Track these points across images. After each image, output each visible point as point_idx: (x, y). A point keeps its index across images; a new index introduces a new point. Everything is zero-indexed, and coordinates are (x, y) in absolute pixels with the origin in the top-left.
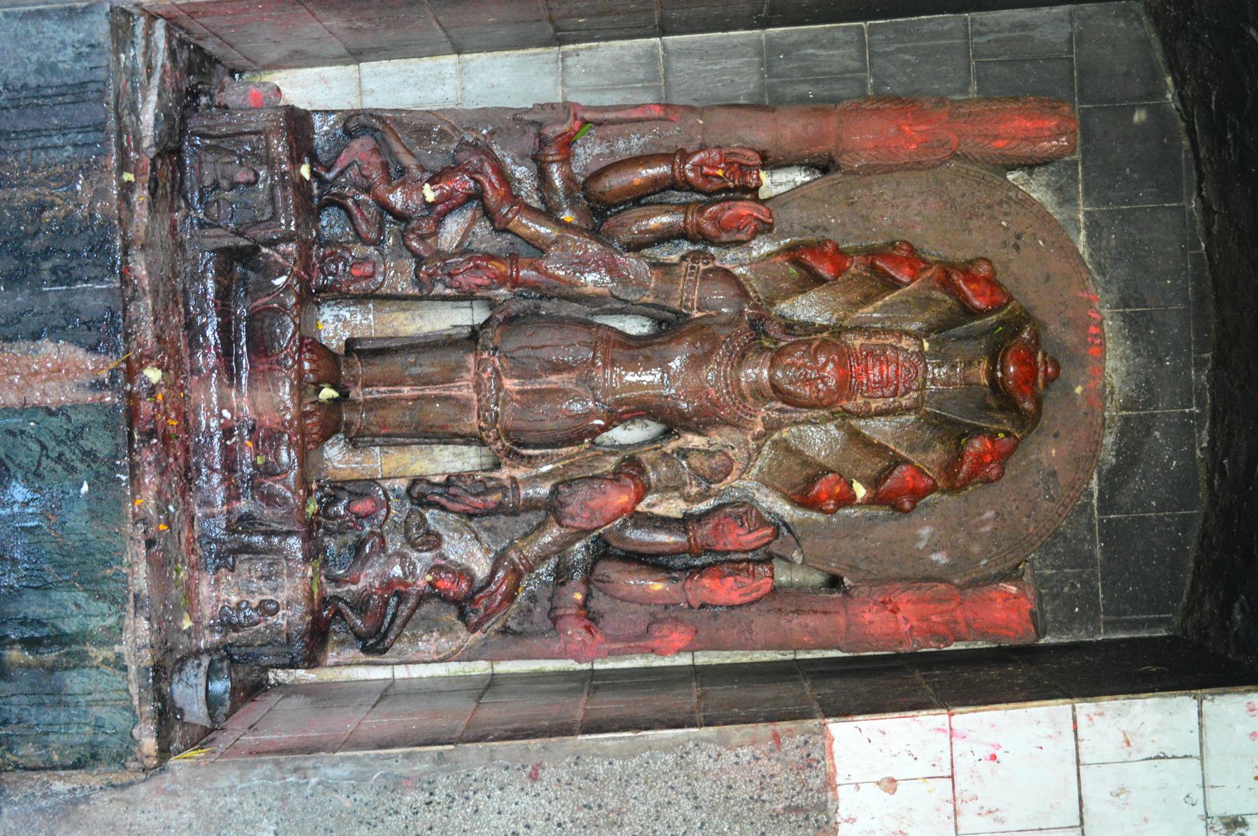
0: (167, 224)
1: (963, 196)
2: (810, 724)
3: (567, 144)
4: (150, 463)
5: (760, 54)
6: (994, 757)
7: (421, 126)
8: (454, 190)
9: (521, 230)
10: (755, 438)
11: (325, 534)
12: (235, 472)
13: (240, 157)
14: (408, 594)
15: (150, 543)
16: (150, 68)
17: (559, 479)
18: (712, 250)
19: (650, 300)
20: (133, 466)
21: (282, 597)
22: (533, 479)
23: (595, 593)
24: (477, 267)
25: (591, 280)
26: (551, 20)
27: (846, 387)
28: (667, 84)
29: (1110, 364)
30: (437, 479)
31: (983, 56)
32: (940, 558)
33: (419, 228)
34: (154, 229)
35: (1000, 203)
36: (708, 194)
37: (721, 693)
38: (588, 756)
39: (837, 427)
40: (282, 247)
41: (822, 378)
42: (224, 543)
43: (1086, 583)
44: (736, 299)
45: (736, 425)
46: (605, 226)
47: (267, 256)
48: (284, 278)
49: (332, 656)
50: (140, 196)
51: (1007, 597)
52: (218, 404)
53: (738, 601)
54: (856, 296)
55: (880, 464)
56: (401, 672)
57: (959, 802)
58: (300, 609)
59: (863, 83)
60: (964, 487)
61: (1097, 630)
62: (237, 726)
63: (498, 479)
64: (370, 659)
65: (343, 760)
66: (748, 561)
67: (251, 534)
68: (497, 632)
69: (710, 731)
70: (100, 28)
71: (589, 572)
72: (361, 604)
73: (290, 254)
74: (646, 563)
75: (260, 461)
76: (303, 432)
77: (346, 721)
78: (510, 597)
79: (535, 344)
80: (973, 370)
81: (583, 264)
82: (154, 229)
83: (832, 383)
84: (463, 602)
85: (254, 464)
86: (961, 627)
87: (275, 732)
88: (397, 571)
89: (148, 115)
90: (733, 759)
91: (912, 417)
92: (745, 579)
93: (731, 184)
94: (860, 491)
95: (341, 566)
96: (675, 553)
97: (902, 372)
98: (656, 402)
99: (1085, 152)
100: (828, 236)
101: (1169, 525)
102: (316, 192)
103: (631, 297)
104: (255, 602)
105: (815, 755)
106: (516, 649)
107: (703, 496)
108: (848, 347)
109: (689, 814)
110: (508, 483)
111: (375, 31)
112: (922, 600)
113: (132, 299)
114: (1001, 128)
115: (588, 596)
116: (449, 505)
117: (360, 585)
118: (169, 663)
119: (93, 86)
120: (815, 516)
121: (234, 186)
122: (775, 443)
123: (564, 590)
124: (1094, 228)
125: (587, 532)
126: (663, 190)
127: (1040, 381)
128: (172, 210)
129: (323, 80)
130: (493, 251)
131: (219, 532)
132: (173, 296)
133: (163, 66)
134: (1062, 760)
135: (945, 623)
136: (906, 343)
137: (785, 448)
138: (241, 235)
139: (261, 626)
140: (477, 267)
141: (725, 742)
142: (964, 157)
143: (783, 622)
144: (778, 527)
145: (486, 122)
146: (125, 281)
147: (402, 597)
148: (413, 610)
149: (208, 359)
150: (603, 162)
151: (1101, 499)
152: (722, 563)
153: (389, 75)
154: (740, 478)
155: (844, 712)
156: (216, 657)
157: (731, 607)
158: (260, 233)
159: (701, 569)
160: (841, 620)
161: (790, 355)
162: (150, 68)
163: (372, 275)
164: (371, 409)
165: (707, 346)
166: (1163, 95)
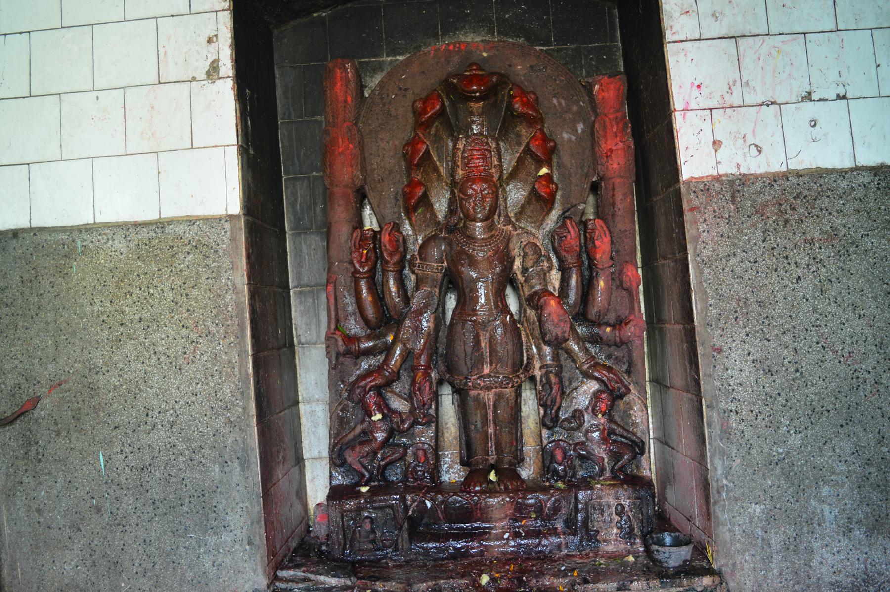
2: (683, 190)
3: (350, 339)
4: (538, 581)
5: (299, 234)
6: (699, 86)
7: (339, 425)
8: (375, 403)
9: (398, 364)
10: (516, 230)
11: (575, 478)
15: (586, 581)
16: (305, 580)
17: (541, 341)
18: (408, 257)
19: (437, 290)
21: (613, 502)
22: (540, 356)
23: (605, 321)
26: (279, 349)
27: (486, 179)
28: (316, 285)
29: (469, 39)
30: (542, 412)
32: (580, 127)
33: (397, 423)
34: (399, 579)
35: (382, 99)
36: (377, 259)
37: (662, 245)
38: (706, 319)
39: (508, 185)
40: (409, 503)
41: (481, 191)
42: (582, 536)
45: (508, 239)
46: (395, 317)
48: (427, 502)
49: (646, 473)
51: (601, 90)
52: (501, 541)
53: (609, 238)
54: (434, 176)
55: (529, 160)
57: (725, 106)
59: (316, 177)
62: (687, 528)
66: (585, 232)
67: (577, 521)
68: (629, 377)
69: (690, 247)
72: (615, 456)
73: (412, 498)
74: (588, 292)
75: (534, 516)
76: (516, 491)
78: (610, 369)
80: (475, 111)
81: (417, 329)
82: (399, 579)
83: (484, 186)
84: (613, 395)
85: (535, 519)
86: (619, 115)
87: (693, 506)
88: (596, 435)
89: (333, 581)
90: (705, 234)
92: (597, 234)
94: (544, 171)
95: (593, 468)
96: (582, 275)
97: (477, 147)
98: (496, 285)
100: (400, 192)
103: (436, 301)
104: (617, 518)
106: (639, 365)
107: (549, 259)
108: (463, 178)
110: (544, 371)
111: (285, 450)
112: (605, 137)
114: (341, 99)
115: (608, 324)
116: (557, 404)
117: (605, 456)
118: (656, 569)
120: (558, 197)
121: (373, 531)
122: (517, 220)
123: (605, 338)
124: (394, 52)
125: (571, 325)
126: (375, 285)
128: (387, 567)
129: (313, 480)
130: (410, 381)
131: (577, 540)
133: (304, 572)
138: (402, 527)
139: (631, 514)
140: (419, 389)
141: (696, 239)
143: (620, 213)
144: (566, 217)
145: (337, 385)
147: (612, 432)
148: (619, 426)
149: (474, 546)
151: (543, 46)
153: (310, 442)
156: (651, 541)
157: (612, 242)
158: (401, 516)
159: (591, 259)
160: (617, 181)
161: (468, 210)
162: (305, 580)
163: (424, 450)
164: (502, 451)
165: (464, 257)
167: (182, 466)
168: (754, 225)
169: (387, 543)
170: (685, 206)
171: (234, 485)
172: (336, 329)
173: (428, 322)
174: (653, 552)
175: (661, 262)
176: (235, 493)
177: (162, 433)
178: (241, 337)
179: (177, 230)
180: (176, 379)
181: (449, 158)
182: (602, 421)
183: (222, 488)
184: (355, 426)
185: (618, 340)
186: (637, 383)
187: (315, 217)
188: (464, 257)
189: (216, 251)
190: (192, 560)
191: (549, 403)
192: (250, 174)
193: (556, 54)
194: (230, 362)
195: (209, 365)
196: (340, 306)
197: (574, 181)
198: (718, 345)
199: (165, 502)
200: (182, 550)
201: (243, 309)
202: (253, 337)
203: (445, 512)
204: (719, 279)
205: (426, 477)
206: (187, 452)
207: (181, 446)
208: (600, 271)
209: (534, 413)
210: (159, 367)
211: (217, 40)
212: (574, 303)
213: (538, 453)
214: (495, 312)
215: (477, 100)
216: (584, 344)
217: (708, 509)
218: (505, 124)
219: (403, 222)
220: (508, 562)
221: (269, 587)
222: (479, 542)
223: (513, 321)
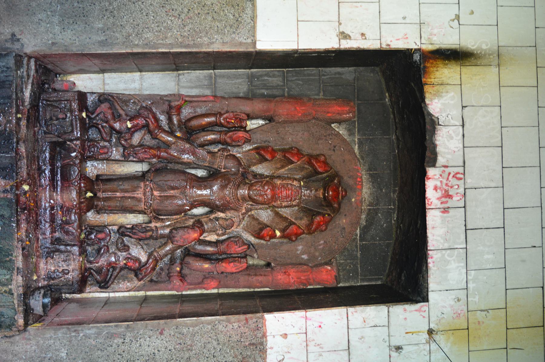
0: (32, 132)
1: (316, 132)
2: (258, 315)
3: (179, 109)
5: (248, 78)
6: (320, 326)
8: (138, 123)
9: (162, 139)
10: (242, 214)
11: (87, 245)
13: (60, 109)
14: (117, 267)
15: (23, 249)
16: (28, 76)
17: (172, 227)
18: (229, 148)
19: (207, 165)
20: (18, 221)
21: (70, 268)
23: (184, 267)
24: (145, 151)
25: (186, 157)
26: (175, 64)
27: (274, 198)
30: (128, 226)
32: (305, 257)
33: (125, 136)
35: (329, 135)
36: (229, 128)
37: (228, 303)
38: (180, 326)
41: (266, 194)
43: (354, 265)
45: (236, 210)
46: (192, 138)
47: (69, 145)
48: (75, 154)
49: (88, 289)
50: (23, 123)
51: (327, 271)
53: (235, 271)
54: (278, 166)
55: (285, 224)
56: (112, 295)
59: (284, 91)
60: (314, 232)
63: (151, 227)
64: (102, 290)
65: (92, 327)
66: (239, 257)
67: (60, 245)
68: (149, 281)
70: (11, 62)
71: (182, 260)
72: (99, 271)
74: (202, 257)
76: (80, 208)
78: (153, 269)
81: (183, 152)
83: (269, 196)
84: (138, 270)
85: (62, 220)
86: (311, 281)
87: (66, 317)
88: (113, 259)
89: (27, 94)
90: (231, 327)
91: (297, 208)
92: (237, 264)
93: (236, 125)
94: (278, 233)
95: (93, 257)
96: (213, 254)
98: (208, 201)
99: (358, 118)
100: (270, 144)
101: (382, 246)
102: (87, 122)
103: (200, 164)
104: (60, 270)
105: (260, 326)
106: (156, 287)
107: (223, 234)
109: (216, 346)
110: (154, 228)
112: (298, 272)
113: (19, 160)
114: (330, 110)
116: (133, 236)
117: (99, 264)
118: (29, 293)
119: (7, 83)
120: (262, 241)
121: (58, 119)
122: (249, 216)
123: (173, 266)
124: (361, 144)
126: (213, 126)
127: (340, 197)
128: (34, 127)
130: (151, 145)
131: (48, 245)
132: (34, 158)
133: (33, 75)
135: (306, 280)
136: (295, 183)
137: (253, 218)
138: (60, 137)
139: (62, 279)
140: (145, 151)
141: (229, 321)
142: (317, 119)
144: (249, 246)
146: (17, 153)
147: (114, 269)
149: (45, 181)
150: (192, 115)
152: (229, 258)
153: (115, 78)
154: (236, 228)
157: (233, 273)
159: (222, 260)
160: (270, 278)
161: (255, 186)
162: (28, 76)
163: (107, 153)
165: (226, 182)
166: (385, 99)
167: (103, 4)
168: (236, 356)
169: (50, 128)
170: (249, 316)
171: (90, 36)
172: (186, 101)
173: (188, 158)
174: (39, 290)
175: (219, 302)
178: (181, 45)
179: (249, 9)
181: (289, 175)
182: (121, 263)
183: (88, 28)
184: (124, 110)
185: (172, 274)
186: (144, 285)
187: (259, 89)
188: (226, 182)
189: (234, 32)
190: (43, 6)
194: (166, 38)
195: (165, 25)
196: (201, 104)
198: (165, 332)
201: (198, 47)
202: (181, 53)
203: (68, 165)
204: (204, 334)
205: (90, 153)
206: (111, 8)
208: (214, 265)
209: (129, 221)
213: (103, 223)
215: (324, 194)
216: (170, 254)
217: (64, 325)
218: (309, 211)
219: (251, 145)
220: (36, 202)
221: (25, 54)
222: (49, 185)
223: (185, 211)
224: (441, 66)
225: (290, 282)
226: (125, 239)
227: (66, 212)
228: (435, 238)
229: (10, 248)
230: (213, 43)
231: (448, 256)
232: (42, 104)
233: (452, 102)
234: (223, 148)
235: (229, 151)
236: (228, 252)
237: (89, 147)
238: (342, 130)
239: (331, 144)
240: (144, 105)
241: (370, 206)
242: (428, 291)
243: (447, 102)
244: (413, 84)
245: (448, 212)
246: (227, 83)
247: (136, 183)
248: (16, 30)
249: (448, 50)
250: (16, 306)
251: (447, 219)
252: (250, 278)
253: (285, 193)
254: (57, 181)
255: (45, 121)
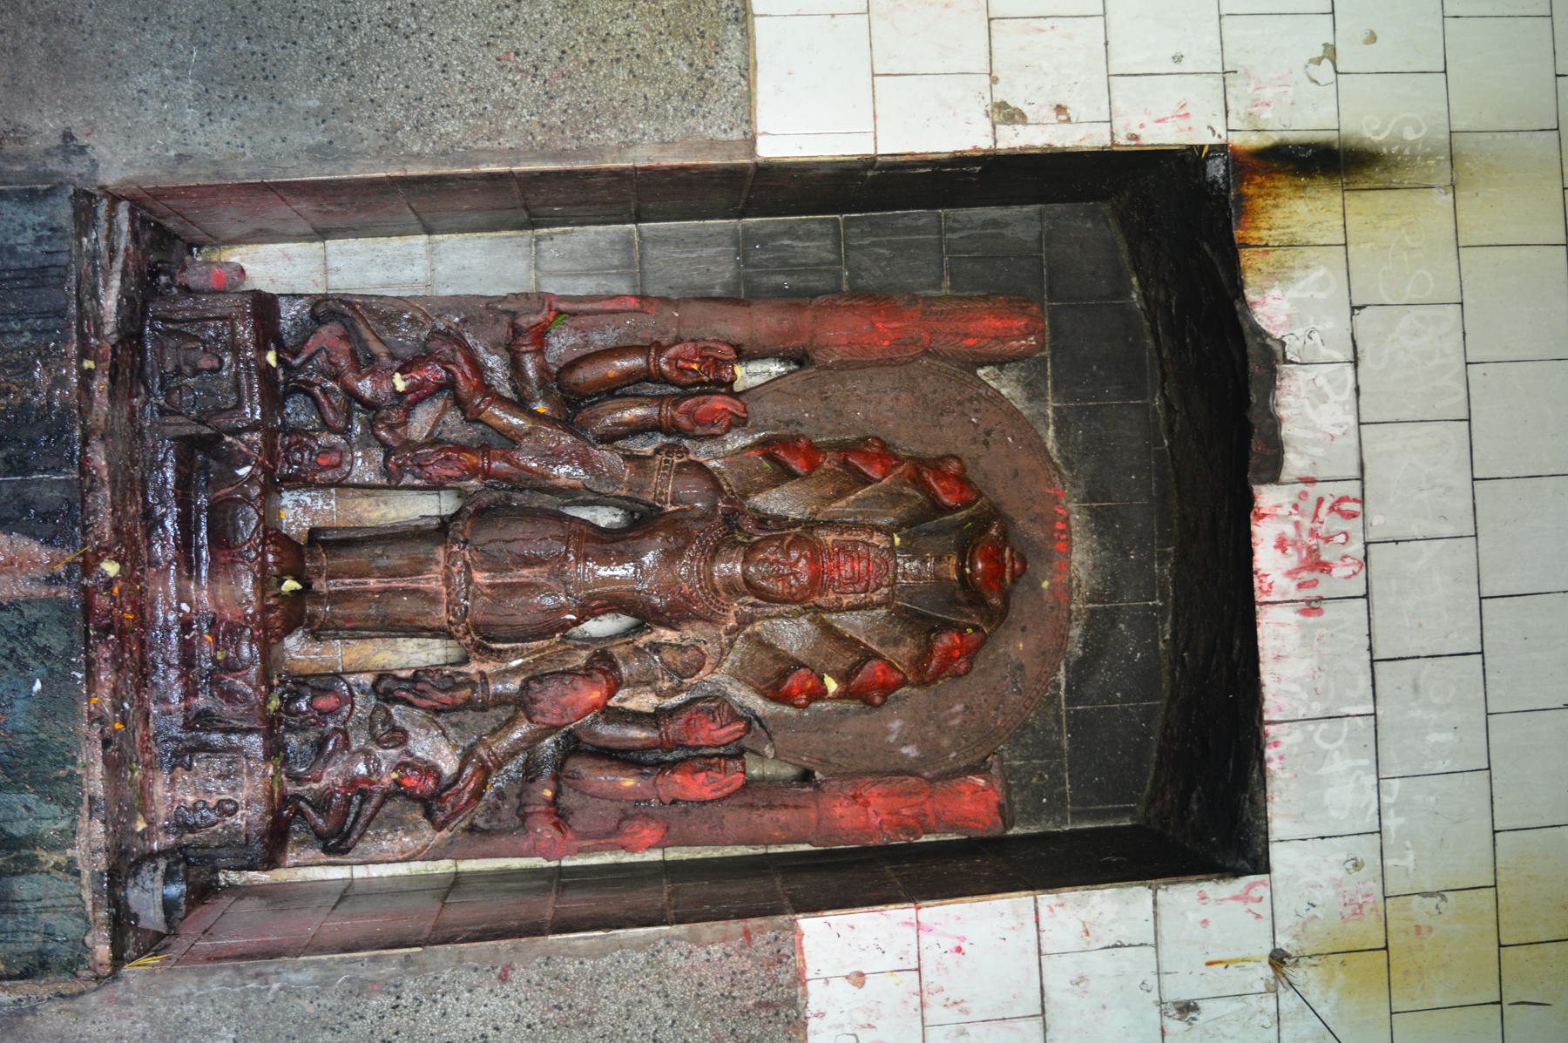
1: (935, 392)
3: (540, 336)
5: (736, 243)
6: (959, 950)
8: (425, 379)
9: (493, 421)
10: (728, 633)
11: (285, 731)
12: (193, 666)
13: (204, 342)
15: (106, 743)
16: (112, 250)
17: (529, 674)
18: (686, 443)
19: (624, 493)
20: (90, 663)
21: (241, 796)
22: (503, 674)
23: (565, 789)
24: (448, 459)
26: (526, 208)
27: (817, 582)
28: (642, 272)
30: (404, 674)
31: (955, 251)
32: (910, 751)
33: (388, 418)
35: (971, 400)
36: (684, 387)
37: (691, 889)
38: (558, 954)
41: (794, 574)
43: (1053, 773)
44: (710, 494)
45: (710, 619)
46: (579, 418)
47: (230, 445)
48: (248, 468)
49: (291, 857)
50: (100, 384)
51: (976, 789)
53: (710, 796)
54: (828, 490)
56: (360, 872)
58: (260, 808)
59: (838, 275)
60: (934, 680)
61: (1064, 821)
63: (467, 674)
65: (306, 964)
66: (720, 756)
67: (209, 732)
68: (464, 830)
70: (63, 212)
71: (559, 766)
72: (322, 803)
73: (256, 443)
74: (617, 759)
75: (220, 656)
76: (265, 625)
77: (306, 924)
78: (477, 795)
79: (507, 537)
81: (556, 457)
83: (804, 579)
84: (430, 799)
85: (214, 659)
86: (931, 820)
87: (232, 937)
88: (361, 769)
89: (110, 301)
90: (705, 956)
91: (883, 611)
94: (832, 685)
95: (303, 763)
96: (646, 748)
98: (629, 597)
100: (802, 430)
102: (281, 378)
103: (605, 490)
104: (212, 802)
105: (786, 951)
106: (485, 848)
107: (675, 691)
108: (820, 543)
111: (344, 213)
112: (890, 794)
113: (91, 490)
114: (972, 327)
115: (557, 793)
116: (417, 701)
117: (323, 783)
119: (54, 271)
120: (787, 710)
121: (197, 372)
122: (748, 636)
123: (533, 787)
124: (1062, 423)
125: (556, 728)
126: (637, 382)
127: (1007, 577)
128: (131, 396)
130: (464, 441)
131: (175, 732)
132: (130, 484)
133: (126, 249)
134: (1025, 951)
135: (913, 817)
136: (877, 539)
137: (759, 642)
138: (203, 423)
139: (219, 828)
141: (696, 940)
142: (935, 355)
144: (749, 723)
146: (83, 472)
147: (365, 796)
148: (377, 809)
149: (163, 550)
150: (578, 353)
151: (1068, 689)
152: (694, 758)
153: (356, 253)
155: (814, 906)
157: (704, 803)
158: (222, 421)
159: (673, 765)
160: (812, 815)
161: (763, 550)
162: (112, 250)
163: (338, 465)
165: (681, 541)
166: (1128, 295)
167: (318, 42)
171: (284, 133)
172: (560, 313)
173: (568, 475)
175: (667, 888)
176: (269, 134)
177: (377, 8)
178: (543, 153)
179: (733, 45)
180: (471, 36)
181: (860, 518)
182: (385, 780)
183: (278, 112)
185: (530, 809)
186: (451, 842)
187: (767, 273)
190: (149, 53)
191: (420, 686)
192: (830, 172)
193: (1051, 712)
194: (500, 133)
195: (495, 95)
196: (602, 319)
197: (814, 737)
199: (254, 8)
200: (169, 36)
201: (592, 158)
202: (544, 175)
204: (627, 978)
206: (342, 51)
207: (354, 41)
210: (494, 6)
211: (1061, 122)
212: (596, 734)
214: (582, 594)
215: (960, 569)
216: (524, 749)
217: (226, 958)
218: (917, 619)
219: (748, 433)
220: (139, 610)
221: (101, 188)
222: (175, 559)
223: (565, 626)
224: (1288, 191)
225: (867, 826)
226: (394, 710)
227: (224, 635)
228: (1283, 686)
229: (69, 741)
230: (634, 144)
231: (1323, 737)
232: (154, 329)
233: (1323, 295)
234: (668, 445)
235: (687, 451)
236: (690, 743)
237: (287, 449)
238: (1007, 386)
239: (976, 426)
240: (441, 326)
241: (1093, 602)
242: (1267, 841)
243: (1306, 295)
244: (1207, 248)
245: (1318, 611)
246: (675, 260)
247: (422, 550)
248: (76, 122)
249: (1307, 146)
250: (89, 908)
251: (1318, 632)
252: (754, 816)
253: (848, 567)
254: (198, 548)
255: (162, 377)
